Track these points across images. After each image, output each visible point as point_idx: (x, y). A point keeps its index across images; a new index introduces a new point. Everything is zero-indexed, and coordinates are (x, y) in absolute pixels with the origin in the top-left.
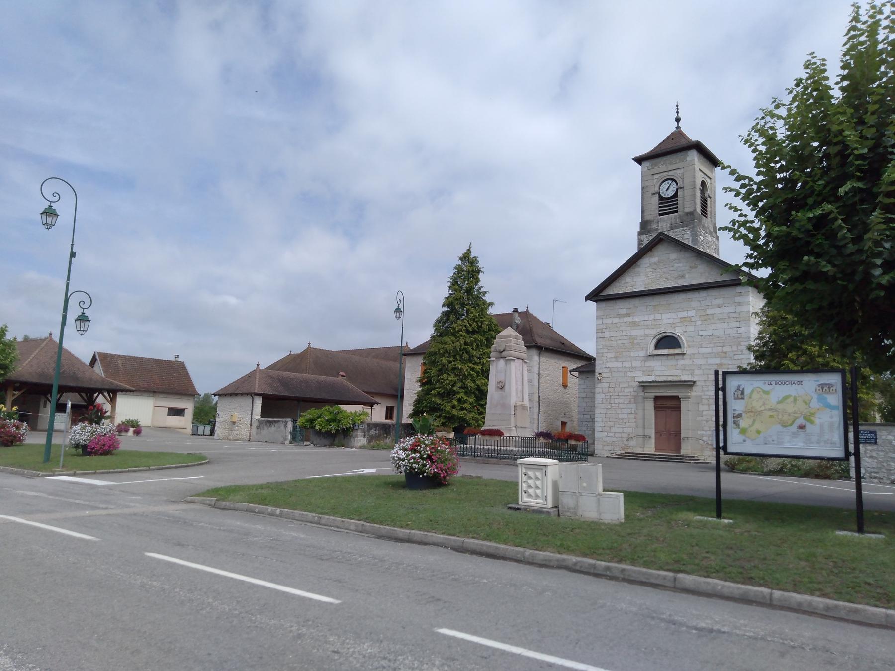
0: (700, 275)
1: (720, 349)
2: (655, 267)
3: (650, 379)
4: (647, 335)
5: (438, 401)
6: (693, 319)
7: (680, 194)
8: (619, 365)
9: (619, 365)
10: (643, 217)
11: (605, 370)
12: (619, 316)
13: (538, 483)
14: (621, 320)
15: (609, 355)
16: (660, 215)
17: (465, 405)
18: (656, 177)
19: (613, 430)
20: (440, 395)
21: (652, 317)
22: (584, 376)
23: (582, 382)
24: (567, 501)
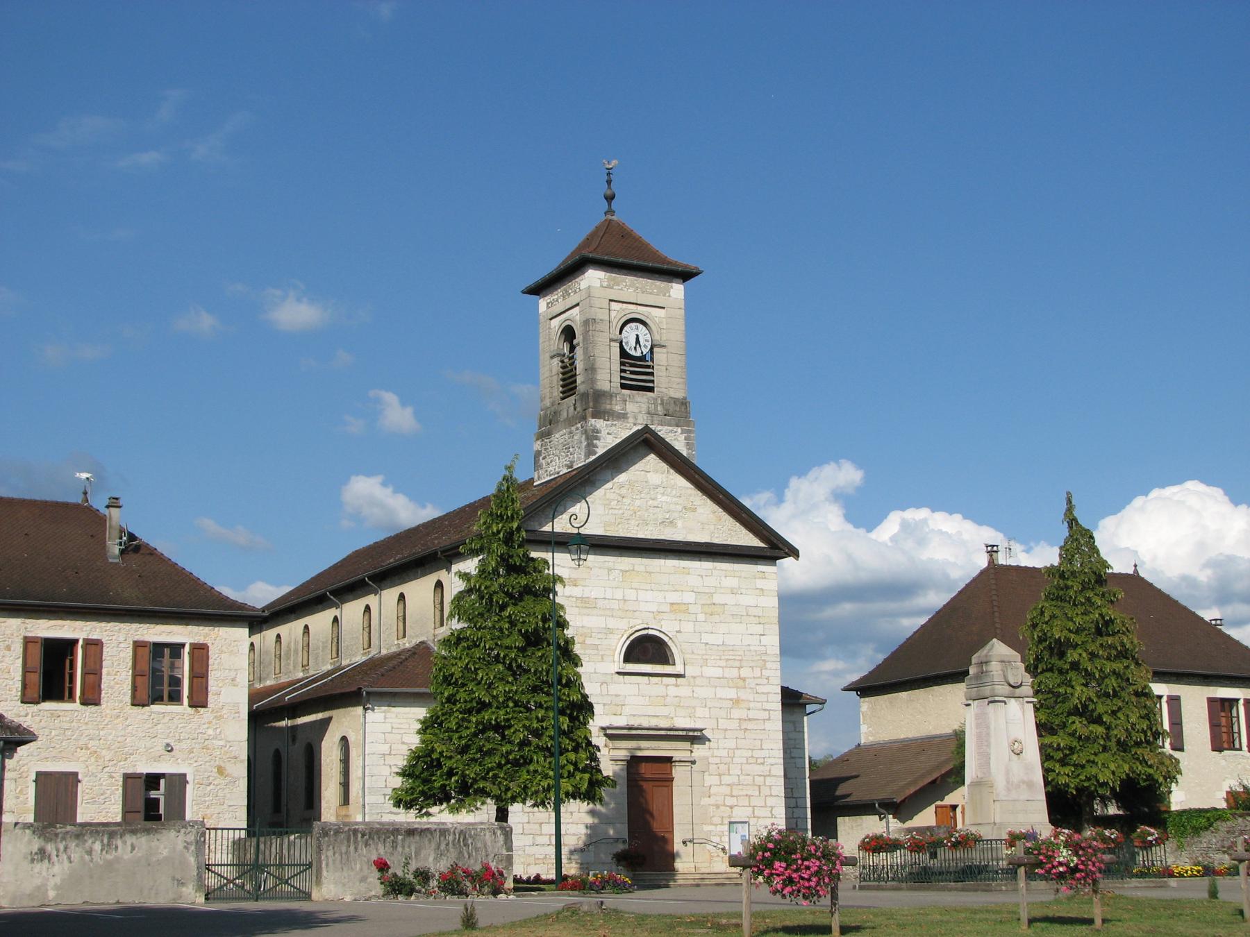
6: (692, 609)
16: (623, 386)
18: (614, 306)
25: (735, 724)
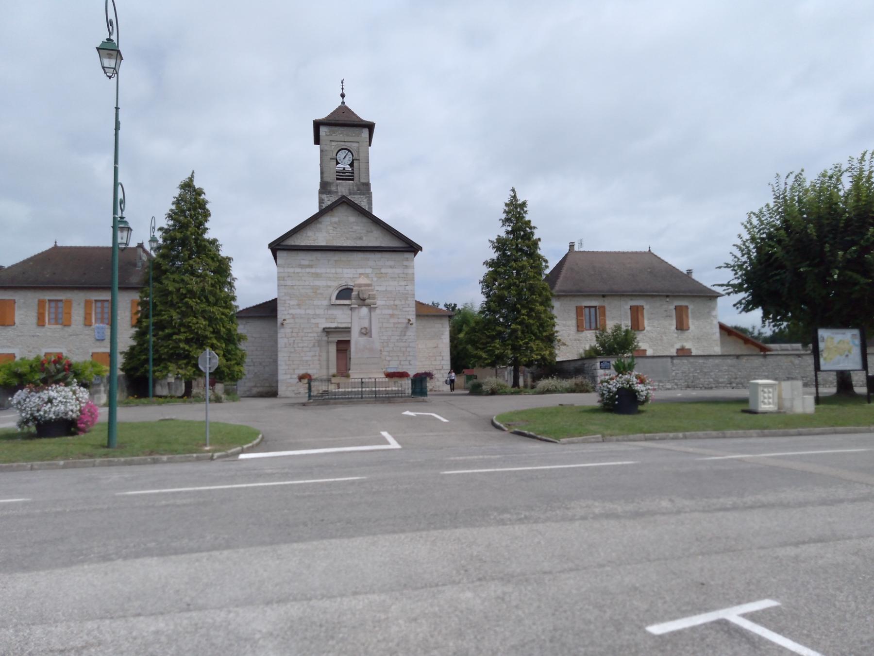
0: (375, 239)
1: (392, 303)
3: (333, 325)
4: (330, 287)
8: (302, 312)
9: (302, 312)
10: (322, 178)
12: (301, 266)
13: (771, 395)
14: (303, 271)
16: (338, 179)
18: (333, 143)
20: (187, 341)
21: (333, 271)
24: (787, 404)
25: (392, 325)
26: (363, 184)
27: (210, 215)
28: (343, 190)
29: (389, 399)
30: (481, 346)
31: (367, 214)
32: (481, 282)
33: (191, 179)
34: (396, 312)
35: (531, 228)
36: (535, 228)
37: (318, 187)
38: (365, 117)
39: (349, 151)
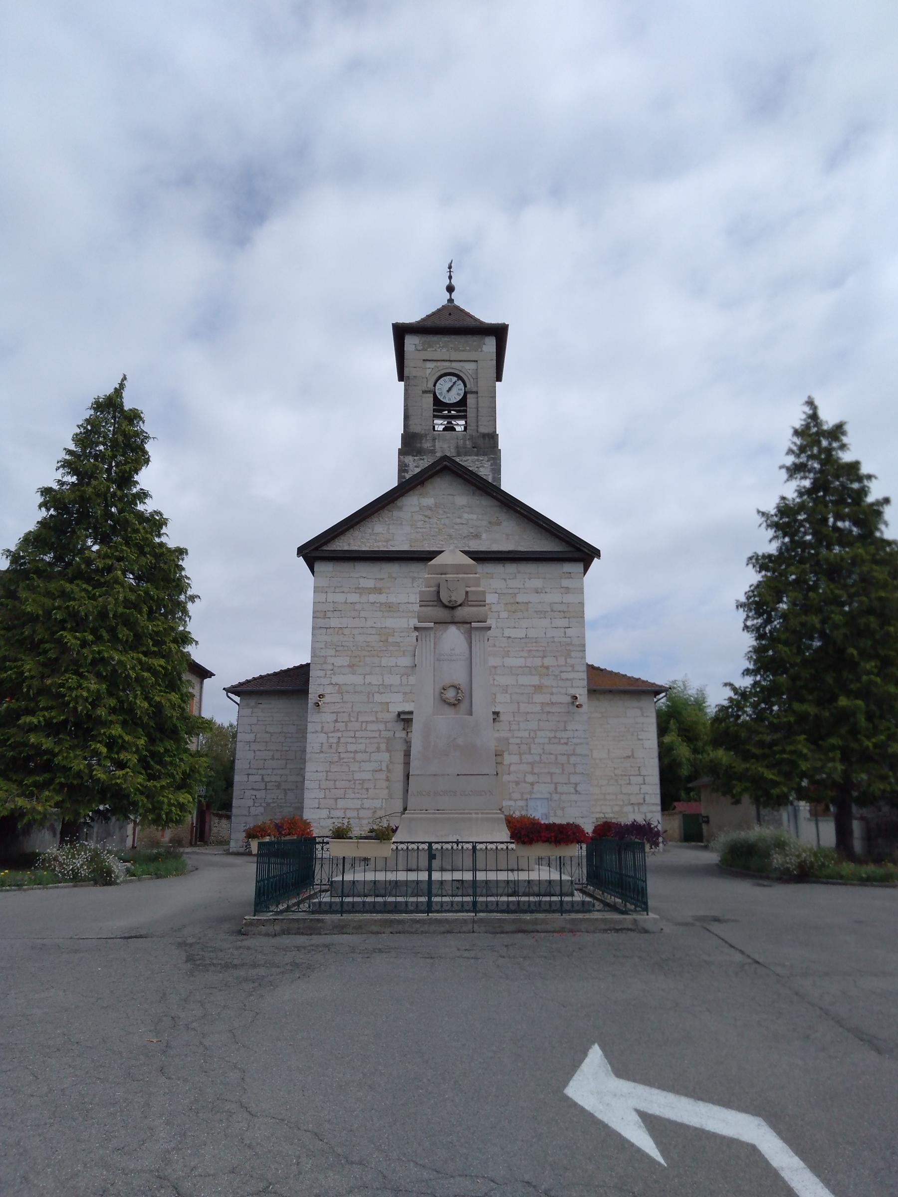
0: (507, 536)
1: (538, 662)
2: (428, 513)
5: (48, 744)
7: (471, 400)
8: (357, 679)
9: (357, 679)
11: (329, 689)
12: (361, 591)
14: (364, 599)
15: (339, 662)
17: (123, 756)
19: (341, 803)
20: (52, 729)
22: (252, 702)
23: (248, 711)
25: (538, 708)
26: (484, 436)
27: (147, 461)
28: (445, 446)
29: (519, 913)
30: (757, 751)
31: (490, 491)
32: (740, 605)
33: (119, 391)
34: (546, 682)
35: (860, 479)
36: (869, 477)
37: (398, 445)
38: (488, 317)
39: (459, 378)
